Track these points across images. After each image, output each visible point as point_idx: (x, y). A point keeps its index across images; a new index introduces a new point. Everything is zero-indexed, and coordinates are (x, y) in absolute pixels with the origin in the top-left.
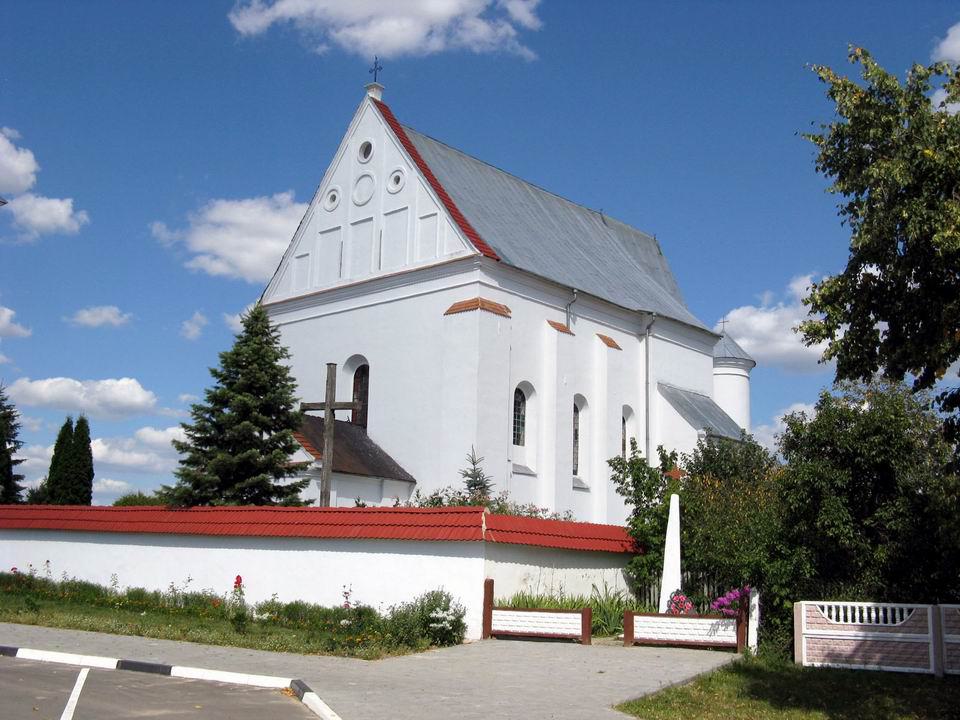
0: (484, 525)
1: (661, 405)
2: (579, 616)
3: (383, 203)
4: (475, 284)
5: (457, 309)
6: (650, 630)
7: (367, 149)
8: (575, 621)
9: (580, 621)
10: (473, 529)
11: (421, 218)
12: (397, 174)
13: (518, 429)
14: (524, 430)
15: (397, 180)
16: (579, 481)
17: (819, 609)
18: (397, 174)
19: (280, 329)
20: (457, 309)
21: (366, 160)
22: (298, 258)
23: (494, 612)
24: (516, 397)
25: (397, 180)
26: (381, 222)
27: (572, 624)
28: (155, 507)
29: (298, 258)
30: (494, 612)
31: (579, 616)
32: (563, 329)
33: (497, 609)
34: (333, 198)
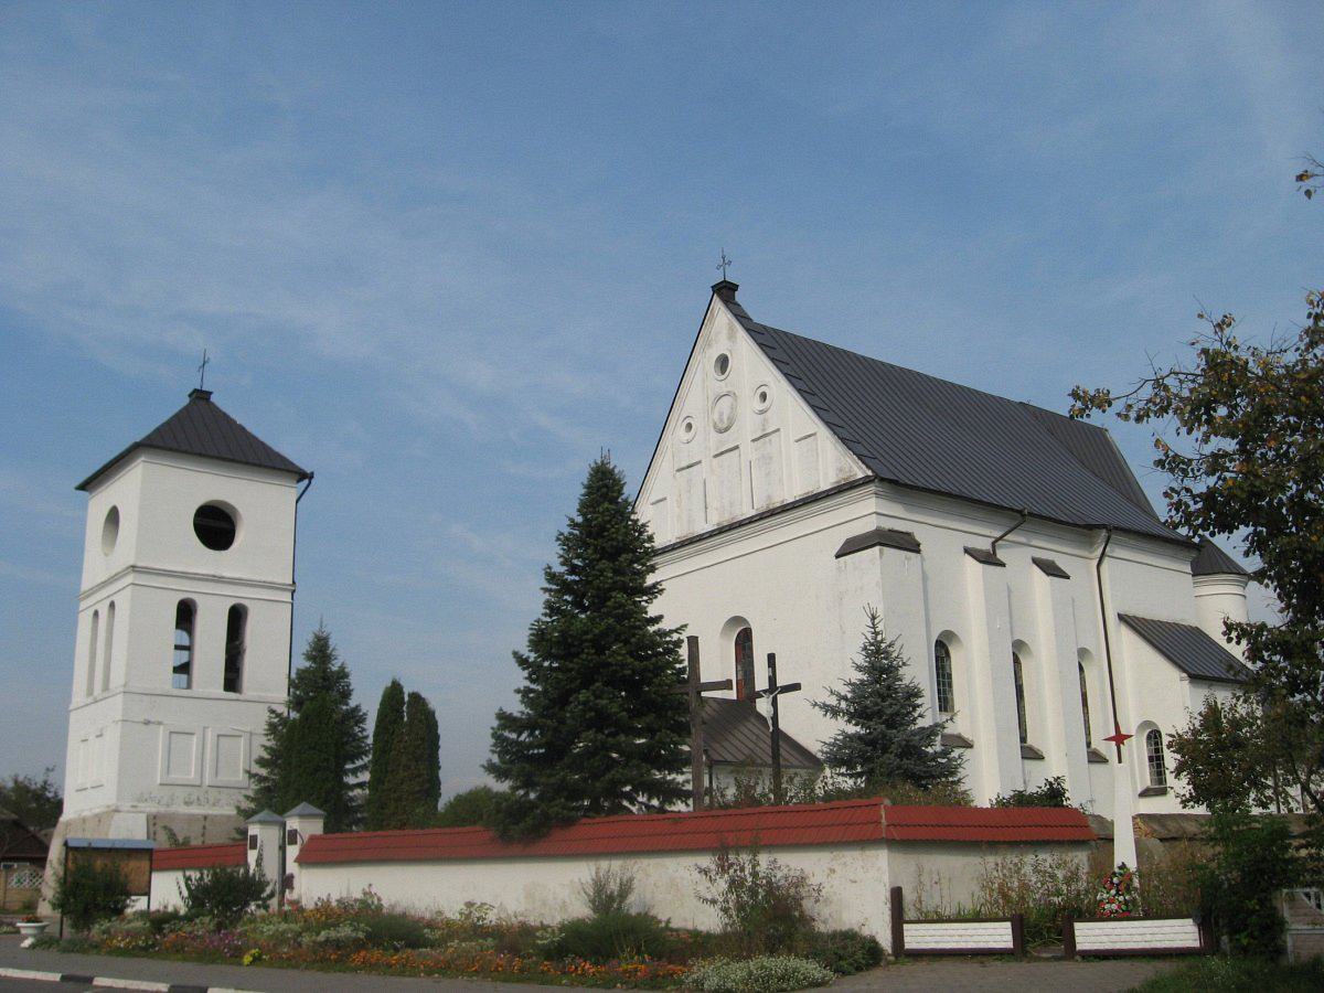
0: (883, 820)
1: (1131, 651)
2: (1008, 924)
3: (747, 426)
4: (867, 512)
5: (851, 547)
6: (1139, 938)
7: (723, 363)
8: (1002, 932)
9: (1010, 931)
10: (872, 826)
11: (797, 441)
12: (688, 421)
13: (944, 691)
14: (951, 691)
15: (764, 397)
16: (1031, 749)
17: (1304, 898)
18: (688, 421)
19: (663, 583)
20: (851, 547)
21: (724, 376)
22: (653, 504)
23: (906, 926)
24: (936, 650)
25: (764, 397)
26: (749, 451)
27: (999, 935)
28: (730, 811)
29: (653, 504)
30: (906, 926)
31: (1008, 924)
32: (989, 559)
33: (908, 922)
34: (689, 426)
